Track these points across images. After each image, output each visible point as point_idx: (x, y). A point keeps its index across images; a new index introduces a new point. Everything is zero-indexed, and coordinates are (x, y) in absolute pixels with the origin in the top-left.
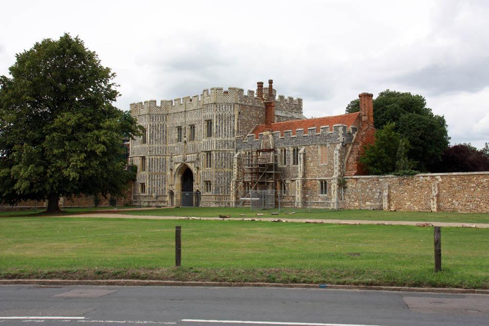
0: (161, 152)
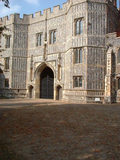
0: (22, 54)
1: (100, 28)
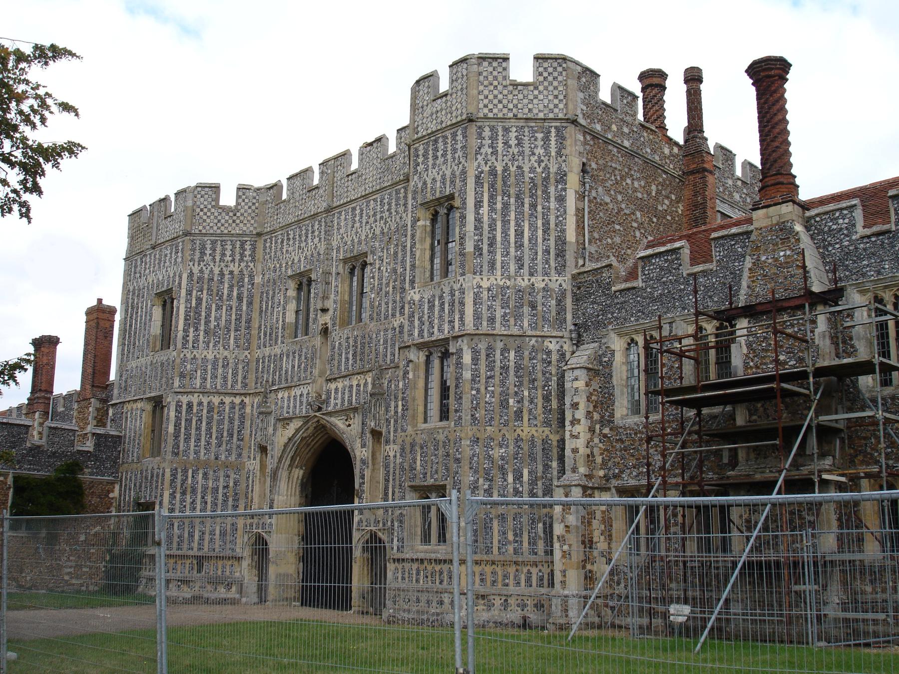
0: (225, 378)
1: (540, 240)
